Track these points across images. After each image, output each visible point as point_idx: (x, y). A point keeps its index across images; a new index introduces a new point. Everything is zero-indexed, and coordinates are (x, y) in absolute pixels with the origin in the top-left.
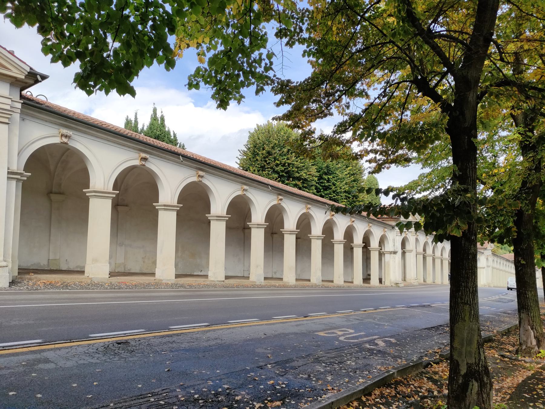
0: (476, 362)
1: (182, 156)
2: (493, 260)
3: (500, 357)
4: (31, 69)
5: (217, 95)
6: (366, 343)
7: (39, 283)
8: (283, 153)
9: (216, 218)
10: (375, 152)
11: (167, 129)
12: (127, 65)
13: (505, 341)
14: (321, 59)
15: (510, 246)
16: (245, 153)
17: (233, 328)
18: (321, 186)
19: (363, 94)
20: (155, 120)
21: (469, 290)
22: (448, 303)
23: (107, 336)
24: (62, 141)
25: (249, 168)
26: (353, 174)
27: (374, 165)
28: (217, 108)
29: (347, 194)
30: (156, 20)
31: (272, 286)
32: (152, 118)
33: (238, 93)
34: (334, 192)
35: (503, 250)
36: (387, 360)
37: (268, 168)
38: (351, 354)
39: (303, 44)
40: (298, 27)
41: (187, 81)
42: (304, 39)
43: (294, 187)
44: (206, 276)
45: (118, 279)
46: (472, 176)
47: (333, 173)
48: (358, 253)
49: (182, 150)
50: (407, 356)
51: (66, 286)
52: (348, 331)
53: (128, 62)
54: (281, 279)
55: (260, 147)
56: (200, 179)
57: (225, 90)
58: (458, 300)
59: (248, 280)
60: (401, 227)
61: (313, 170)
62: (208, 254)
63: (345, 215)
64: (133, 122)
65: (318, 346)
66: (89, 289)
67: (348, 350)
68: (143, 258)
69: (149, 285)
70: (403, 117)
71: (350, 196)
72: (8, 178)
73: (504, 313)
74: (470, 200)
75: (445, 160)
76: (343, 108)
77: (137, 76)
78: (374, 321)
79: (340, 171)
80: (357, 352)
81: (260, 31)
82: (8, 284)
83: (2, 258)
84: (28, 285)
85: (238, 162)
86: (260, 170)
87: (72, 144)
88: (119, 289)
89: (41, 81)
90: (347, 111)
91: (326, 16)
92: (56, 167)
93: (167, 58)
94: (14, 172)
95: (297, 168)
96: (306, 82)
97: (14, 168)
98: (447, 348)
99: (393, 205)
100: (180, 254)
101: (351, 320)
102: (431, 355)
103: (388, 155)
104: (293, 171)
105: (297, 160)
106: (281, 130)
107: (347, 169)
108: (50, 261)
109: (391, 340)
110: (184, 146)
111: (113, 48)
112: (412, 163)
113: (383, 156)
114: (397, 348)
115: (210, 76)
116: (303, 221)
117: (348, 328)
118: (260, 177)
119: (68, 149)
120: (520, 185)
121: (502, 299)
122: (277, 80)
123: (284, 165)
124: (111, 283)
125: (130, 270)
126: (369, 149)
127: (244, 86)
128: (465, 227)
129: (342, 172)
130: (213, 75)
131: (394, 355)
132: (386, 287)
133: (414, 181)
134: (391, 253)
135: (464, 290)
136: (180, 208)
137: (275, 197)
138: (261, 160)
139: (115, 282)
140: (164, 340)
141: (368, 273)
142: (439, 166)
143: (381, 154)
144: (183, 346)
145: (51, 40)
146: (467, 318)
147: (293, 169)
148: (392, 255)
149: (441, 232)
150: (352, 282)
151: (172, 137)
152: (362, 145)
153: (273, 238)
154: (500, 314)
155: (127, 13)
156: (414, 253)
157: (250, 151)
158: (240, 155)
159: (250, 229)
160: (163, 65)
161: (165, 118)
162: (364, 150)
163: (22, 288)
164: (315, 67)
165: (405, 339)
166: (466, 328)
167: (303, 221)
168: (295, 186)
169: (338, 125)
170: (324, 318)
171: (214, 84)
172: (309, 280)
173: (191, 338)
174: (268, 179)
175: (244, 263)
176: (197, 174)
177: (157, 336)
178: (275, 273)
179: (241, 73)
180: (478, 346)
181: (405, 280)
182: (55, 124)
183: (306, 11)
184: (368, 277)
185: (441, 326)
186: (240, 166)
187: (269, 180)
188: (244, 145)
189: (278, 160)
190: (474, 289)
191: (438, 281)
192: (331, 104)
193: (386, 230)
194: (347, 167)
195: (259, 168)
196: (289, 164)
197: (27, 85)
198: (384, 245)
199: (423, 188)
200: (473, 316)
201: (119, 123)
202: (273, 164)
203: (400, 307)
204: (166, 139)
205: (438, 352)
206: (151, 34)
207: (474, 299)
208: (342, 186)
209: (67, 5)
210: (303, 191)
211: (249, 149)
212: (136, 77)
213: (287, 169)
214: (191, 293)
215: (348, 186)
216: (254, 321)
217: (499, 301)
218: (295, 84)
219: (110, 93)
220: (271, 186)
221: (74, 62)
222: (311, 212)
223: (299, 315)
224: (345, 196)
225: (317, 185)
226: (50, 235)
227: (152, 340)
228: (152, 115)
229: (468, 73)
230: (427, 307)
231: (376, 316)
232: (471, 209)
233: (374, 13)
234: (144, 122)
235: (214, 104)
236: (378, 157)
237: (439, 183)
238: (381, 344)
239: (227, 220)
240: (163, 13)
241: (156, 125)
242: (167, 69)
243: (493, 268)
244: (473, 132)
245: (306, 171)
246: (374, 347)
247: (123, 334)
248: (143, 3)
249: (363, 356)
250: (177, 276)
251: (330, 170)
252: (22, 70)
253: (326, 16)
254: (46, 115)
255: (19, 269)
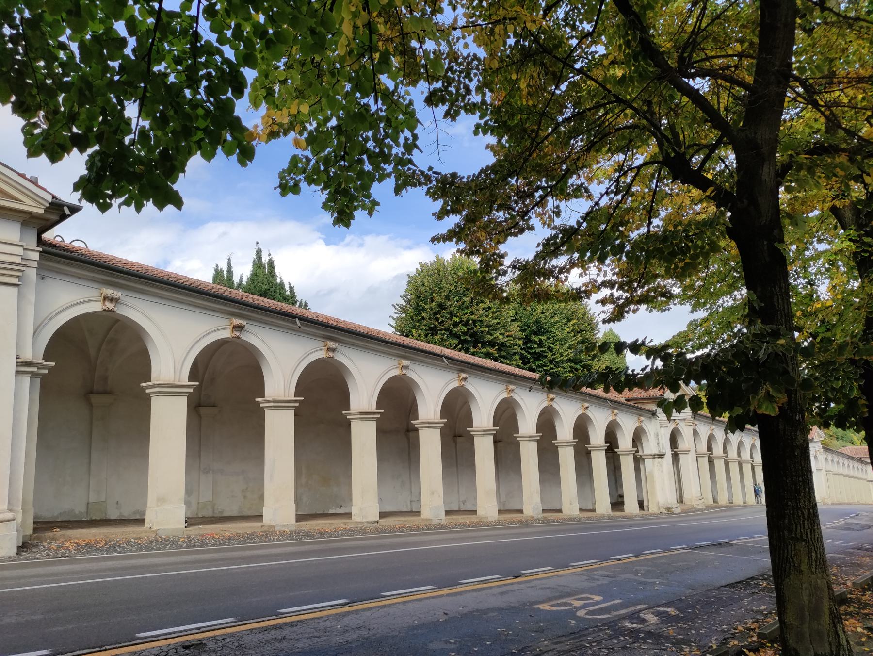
0: (832, 652)
1: (300, 319)
2: (826, 459)
3: (865, 632)
4: (54, 197)
5: (331, 202)
6: (624, 618)
7: (68, 544)
8: (463, 304)
9: (359, 416)
10: (610, 284)
11: (278, 281)
12: (164, 154)
13: (869, 600)
14: (506, 138)
15: (858, 431)
16: (403, 309)
17: (390, 605)
18: (529, 353)
19: (580, 191)
20: (259, 267)
21: (803, 514)
22: (763, 538)
23: (166, 634)
24: (104, 308)
25: (410, 331)
26: (580, 331)
27: (610, 307)
28: (334, 224)
29: (573, 365)
30: (213, 77)
31: (460, 525)
32: (254, 264)
33: (368, 196)
34: (551, 362)
35: (841, 441)
36: (665, 650)
37: (441, 330)
38: (599, 642)
39: (473, 113)
40: (462, 86)
41: (277, 182)
42: (474, 105)
43: (485, 358)
44: (348, 515)
45: (201, 529)
46: (784, 308)
47: (548, 332)
48: (599, 461)
49: (304, 310)
50: (700, 640)
51: (113, 546)
52: (592, 599)
53: (166, 150)
54: (474, 512)
55: (426, 298)
56: (331, 354)
57: (346, 192)
58: (783, 533)
59: (418, 518)
60: (668, 408)
61: (515, 328)
62: (349, 477)
63: (566, 391)
64: (225, 273)
65: (541, 630)
66: (152, 549)
67: (594, 635)
68: (243, 491)
69: (252, 536)
70: (652, 229)
71: (578, 367)
72: (17, 372)
73: (859, 549)
74: (786, 350)
75: (729, 297)
76: (550, 216)
77: (184, 172)
78: (636, 578)
79: (559, 328)
80: (611, 637)
81: (401, 100)
82: (15, 550)
83: (5, 506)
84: (49, 549)
85: (393, 323)
86: (428, 334)
87: (122, 311)
88: (202, 546)
89: (69, 216)
90: (557, 222)
91: (507, 66)
92: (99, 349)
93: (240, 145)
94: (26, 363)
95: (488, 326)
96: (483, 175)
97: (27, 356)
98: (769, 619)
99: (648, 370)
100: (303, 480)
101: (596, 577)
102: (744, 635)
103: (632, 289)
104: (482, 332)
105: (487, 314)
106: (458, 269)
107: (569, 324)
108: (90, 505)
109: (668, 610)
110: (306, 305)
111: (139, 127)
112: (675, 304)
113: (625, 291)
114: (679, 625)
115: (316, 170)
116: (504, 412)
117: (591, 594)
118: (429, 345)
119: (117, 321)
120: (862, 327)
121: (851, 524)
122: (436, 176)
123: (466, 323)
124: (189, 537)
125: (221, 512)
126: (600, 280)
127: (374, 181)
128: (783, 398)
129: (562, 329)
130: (322, 168)
131: (677, 639)
132: (651, 515)
133: (680, 333)
134: (654, 456)
135: (793, 514)
136: (194, 389)
137: (455, 375)
138: (430, 319)
139: (197, 535)
140: (268, 636)
141: (619, 493)
142: (719, 306)
143: (621, 287)
144: (300, 645)
145: (39, 127)
146: (804, 567)
147: (482, 329)
148: (657, 460)
149: (739, 411)
150: (594, 511)
151: (288, 293)
152: (586, 274)
153: (456, 444)
154: (852, 551)
155: (163, 70)
156: (693, 454)
157: (411, 305)
158: (395, 313)
159: (416, 430)
160: (234, 158)
161: (275, 263)
162: (590, 282)
163: (38, 556)
164: (499, 155)
165: (693, 607)
166: (804, 585)
167: (504, 412)
168: (488, 355)
169: (543, 243)
170: (548, 578)
171: (325, 183)
172: (521, 511)
173: (315, 628)
174: (443, 347)
175: (411, 489)
176: (325, 346)
177: (255, 629)
178: (464, 502)
179: (365, 157)
180: (833, 621)
181: (682, 502)
182: (94, 281)
183: (473, 60)
184: (620, 500)
185: (752, 579)
186: (397, 330)
187: (444, 349)
188: (401, 297)
189: (457, 317)
190: (811, 511)
191: (738, 500)
192: (529, 211)
193: (642, 418)
194: (569, 320)
195: (426, 330)
196: (474, 322)
197: (49, 223)
198: (642, 444)
199: (696, 343)
200: (816, 562)
201: (203, 275)
202: (448, 323)
203: (678, 549)
204: (277, 295)
205: (754, 629)
206: (208, 104)
207: (813, 531)
208: (564, 352)
209: (59, 61)
210: (501, 362)
211: (409, 302)
212: (181, 175)
213: (472, 329)
214: (322, 547)
215: (573, 350)
216: (427, 591)
217: (845, 529)
218: (465, 180)
219: (143, 209)
220: (447, 358)
221: (68, 154)
222: (516, 397)
223: (505, 574)
224: (570, 367)
225: (523, 352)
226: (90, 463)
227: (245, 637)
228: (254, 261)
229: (756, 133)
230: (724, 547)
231: (638, 568)
232: (788, 367)
233: (587, 61)
234: (243, 272)
235: (328, 218)
236: (617, 293)
237: (722, 334)
238: (652, 619)
239: (377, 418)
240: (222, 63)
241: (262, 276)
242: (243, 164)
243: (827, 472)
244: (776, 232)
245: (503, 331)
246: (639, 626)
247: (196, 629)
248: (188, 50)
249: (621, 644)
250: (300, 518)
251: (541, 328)
252: (41, 201)
253: (507, 66)
254: (79, 267)
255: (35, 523)
